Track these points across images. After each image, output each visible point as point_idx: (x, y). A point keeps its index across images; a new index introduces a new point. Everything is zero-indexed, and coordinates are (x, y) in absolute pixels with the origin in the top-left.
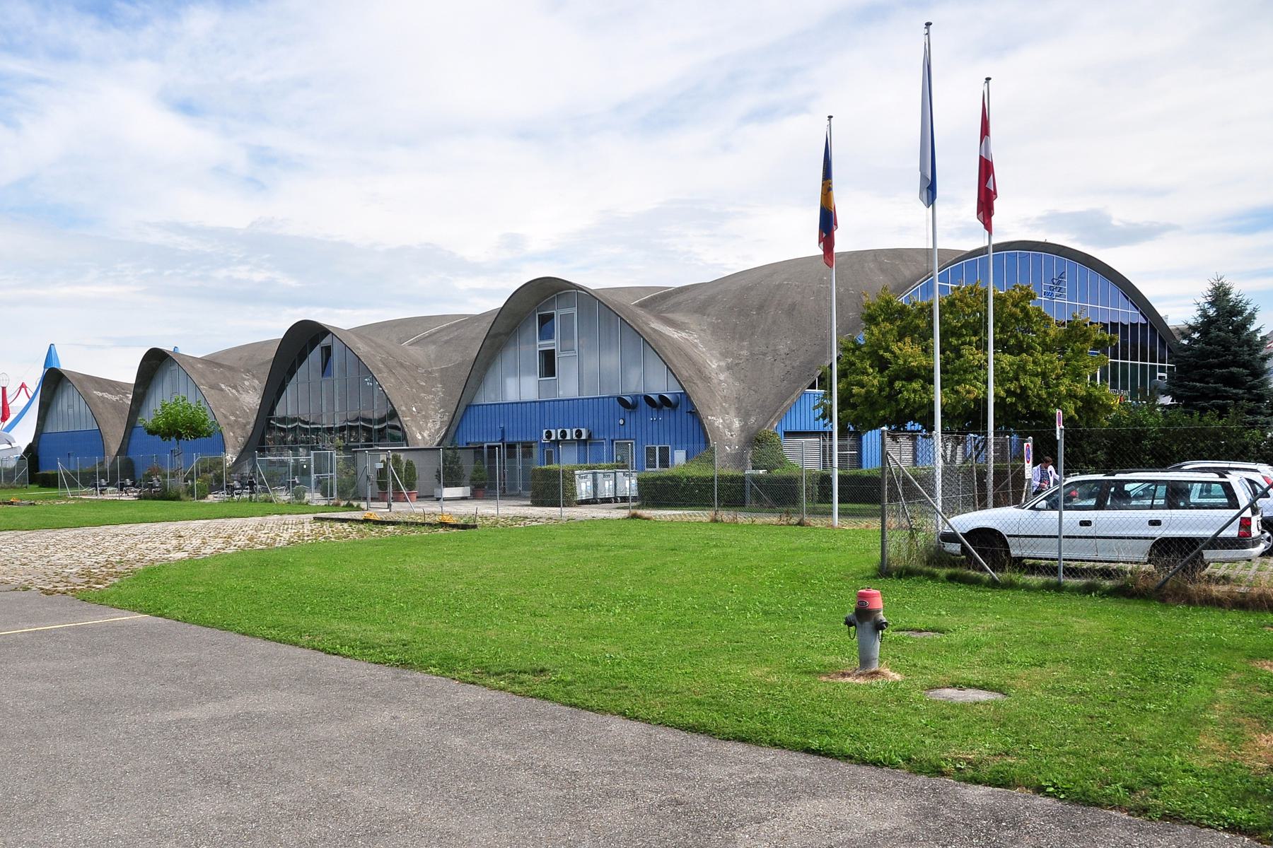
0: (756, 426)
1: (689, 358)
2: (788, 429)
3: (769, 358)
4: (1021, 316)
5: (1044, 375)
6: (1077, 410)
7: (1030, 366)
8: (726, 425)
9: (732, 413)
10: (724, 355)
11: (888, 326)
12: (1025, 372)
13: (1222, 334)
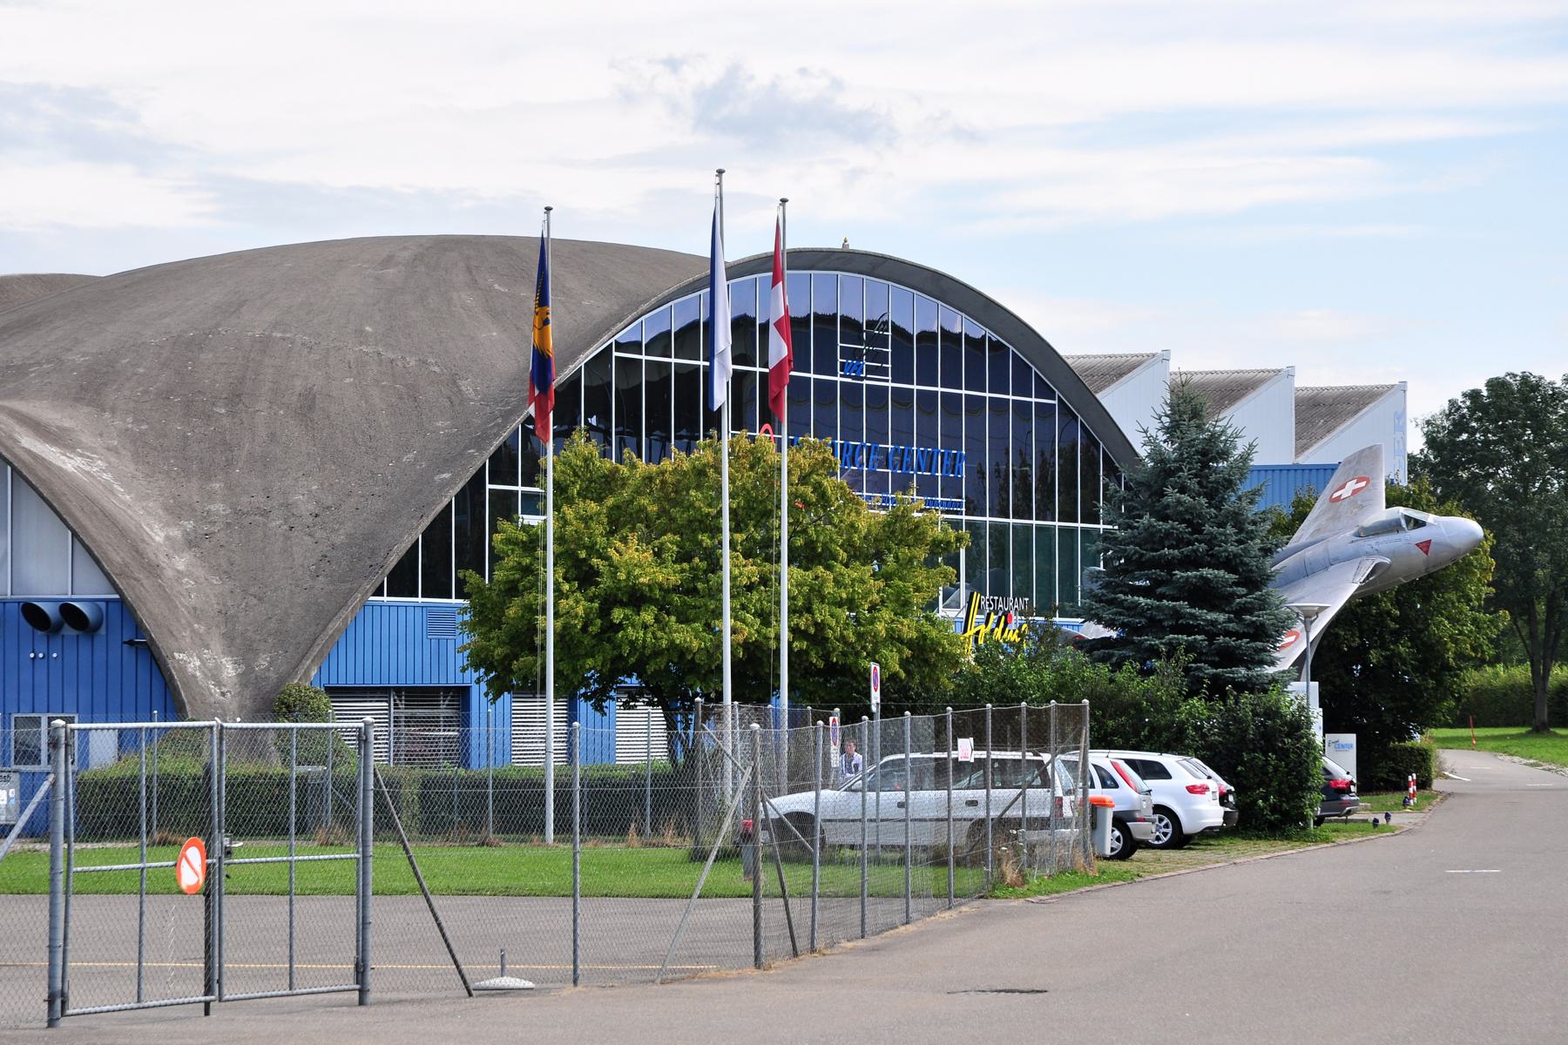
0: (273, 675)
1: (123, 533)
2: (333, 683)
3: (276, 523)
4: (813, 498)
5: (851, 604)
6: (904, 663)
7: (830, 588)
8: (207, 666)
9: (217, 645)
10: (175, 511)
11: (593, 507)
12: (822, 599)
13: (1185, 498)
